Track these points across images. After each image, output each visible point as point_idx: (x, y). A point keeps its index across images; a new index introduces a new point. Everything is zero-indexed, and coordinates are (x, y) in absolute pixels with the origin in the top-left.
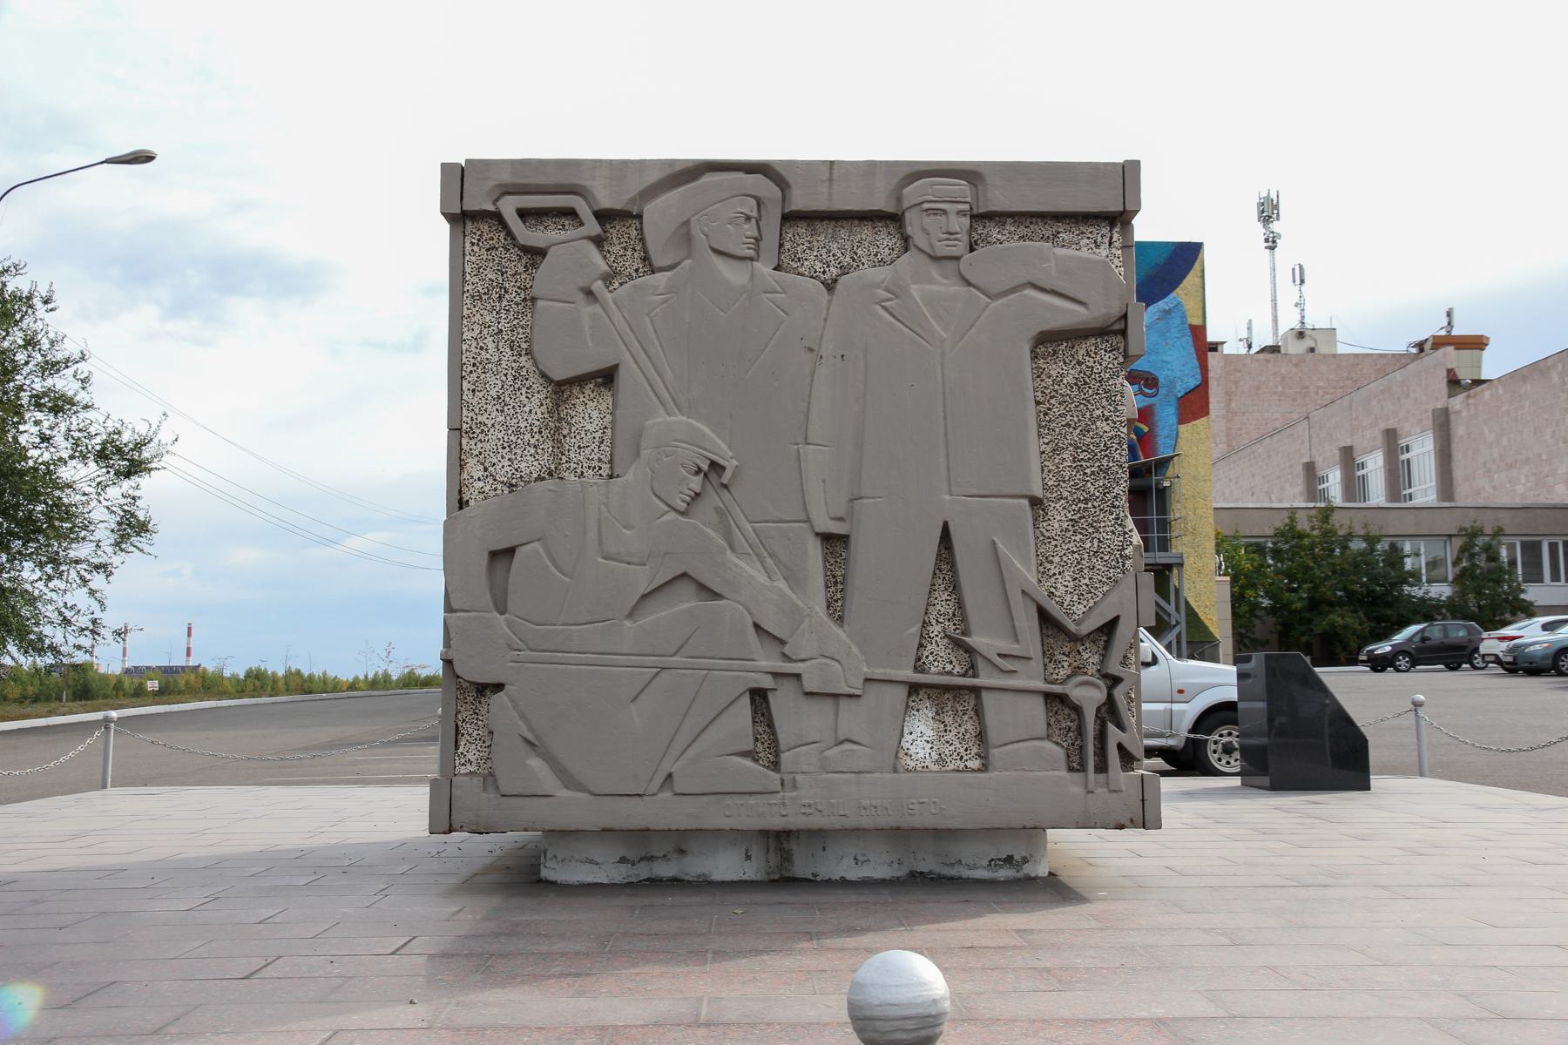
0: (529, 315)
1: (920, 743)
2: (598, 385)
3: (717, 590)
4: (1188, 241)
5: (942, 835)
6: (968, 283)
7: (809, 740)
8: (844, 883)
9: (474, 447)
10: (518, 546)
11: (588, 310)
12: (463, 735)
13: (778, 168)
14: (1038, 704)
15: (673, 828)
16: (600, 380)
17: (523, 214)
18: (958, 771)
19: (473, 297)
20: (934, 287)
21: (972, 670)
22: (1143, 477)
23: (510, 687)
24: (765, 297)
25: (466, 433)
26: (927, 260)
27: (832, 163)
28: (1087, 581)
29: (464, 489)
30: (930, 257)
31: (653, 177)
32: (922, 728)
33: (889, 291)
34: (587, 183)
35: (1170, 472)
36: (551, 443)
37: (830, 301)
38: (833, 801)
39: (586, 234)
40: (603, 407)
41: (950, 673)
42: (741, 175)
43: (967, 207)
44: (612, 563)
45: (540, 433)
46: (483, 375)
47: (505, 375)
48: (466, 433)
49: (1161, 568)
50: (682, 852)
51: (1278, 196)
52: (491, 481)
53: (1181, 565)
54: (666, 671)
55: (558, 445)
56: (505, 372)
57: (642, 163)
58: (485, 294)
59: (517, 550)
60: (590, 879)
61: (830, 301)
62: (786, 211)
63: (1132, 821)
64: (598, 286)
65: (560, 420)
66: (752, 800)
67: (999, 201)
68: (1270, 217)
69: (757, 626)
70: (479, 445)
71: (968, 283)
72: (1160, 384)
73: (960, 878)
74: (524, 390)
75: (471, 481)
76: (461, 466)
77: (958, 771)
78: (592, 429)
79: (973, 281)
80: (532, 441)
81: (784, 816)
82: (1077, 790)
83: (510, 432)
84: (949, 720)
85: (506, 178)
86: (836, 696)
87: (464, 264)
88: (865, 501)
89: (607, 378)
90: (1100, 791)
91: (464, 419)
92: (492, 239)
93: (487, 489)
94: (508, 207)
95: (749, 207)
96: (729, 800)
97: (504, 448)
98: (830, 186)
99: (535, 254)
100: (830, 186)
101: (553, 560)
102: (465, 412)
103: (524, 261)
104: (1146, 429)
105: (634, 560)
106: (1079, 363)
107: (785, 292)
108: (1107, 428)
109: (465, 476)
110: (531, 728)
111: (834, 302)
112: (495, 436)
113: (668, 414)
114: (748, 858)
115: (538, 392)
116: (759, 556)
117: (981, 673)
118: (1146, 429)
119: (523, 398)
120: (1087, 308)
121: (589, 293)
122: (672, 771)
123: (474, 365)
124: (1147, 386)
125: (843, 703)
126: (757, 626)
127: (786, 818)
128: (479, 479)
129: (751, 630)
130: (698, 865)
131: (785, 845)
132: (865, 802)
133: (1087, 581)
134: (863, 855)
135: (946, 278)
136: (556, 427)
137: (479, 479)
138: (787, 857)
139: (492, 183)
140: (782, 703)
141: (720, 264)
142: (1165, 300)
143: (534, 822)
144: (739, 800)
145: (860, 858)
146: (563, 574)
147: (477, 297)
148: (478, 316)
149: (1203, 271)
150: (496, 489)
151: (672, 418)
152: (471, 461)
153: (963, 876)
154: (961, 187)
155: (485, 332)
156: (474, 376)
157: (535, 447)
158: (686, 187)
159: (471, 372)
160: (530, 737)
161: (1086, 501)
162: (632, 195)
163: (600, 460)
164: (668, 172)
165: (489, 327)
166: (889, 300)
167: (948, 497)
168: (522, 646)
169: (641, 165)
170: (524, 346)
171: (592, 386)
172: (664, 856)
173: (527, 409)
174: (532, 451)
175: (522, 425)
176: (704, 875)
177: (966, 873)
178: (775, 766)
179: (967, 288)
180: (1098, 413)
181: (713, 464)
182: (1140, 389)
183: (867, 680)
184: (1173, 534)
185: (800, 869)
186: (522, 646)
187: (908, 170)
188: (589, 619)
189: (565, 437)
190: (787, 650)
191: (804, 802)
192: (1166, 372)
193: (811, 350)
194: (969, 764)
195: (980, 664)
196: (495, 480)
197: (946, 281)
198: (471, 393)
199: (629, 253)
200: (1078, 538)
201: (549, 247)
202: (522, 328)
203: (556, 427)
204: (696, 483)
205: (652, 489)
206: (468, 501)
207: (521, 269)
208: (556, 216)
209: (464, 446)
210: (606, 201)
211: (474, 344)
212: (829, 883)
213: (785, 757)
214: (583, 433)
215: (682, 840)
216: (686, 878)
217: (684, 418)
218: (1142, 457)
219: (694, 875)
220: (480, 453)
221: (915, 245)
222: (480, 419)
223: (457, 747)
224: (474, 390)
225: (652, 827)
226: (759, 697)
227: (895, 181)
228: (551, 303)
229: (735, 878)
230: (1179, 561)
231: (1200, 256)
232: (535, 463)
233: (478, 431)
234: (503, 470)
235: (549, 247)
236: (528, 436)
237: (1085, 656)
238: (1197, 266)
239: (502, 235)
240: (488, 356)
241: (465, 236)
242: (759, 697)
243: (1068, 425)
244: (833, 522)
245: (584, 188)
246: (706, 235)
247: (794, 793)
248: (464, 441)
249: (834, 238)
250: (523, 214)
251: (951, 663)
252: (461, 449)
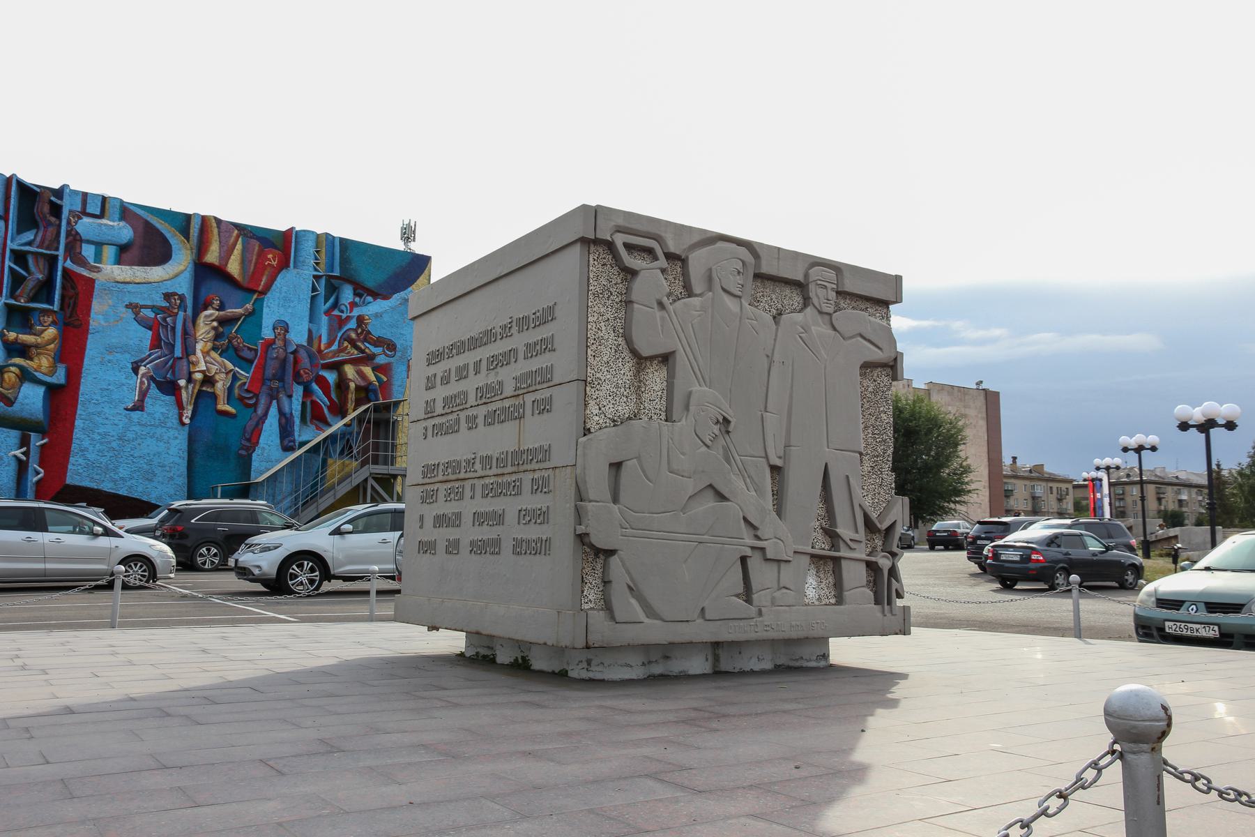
0: (624, 311)
1: (811, 589)
2: (659, 362)
3: (727, 495)
4: (421, 253)
5: (789, 642)
6: (835, 329)
7: (766, 587)
8: (752, 673)
9: (594, 394)
10: (624, 461)
11: (658, 314)
12: (586, 583)
13: (755, 246)
14: (863, 567)
15: (704, 641)
16: (660, 359)
17: (626, 246)
18: (826, 605)
19: (594, 294)
20: (819, 329)
21: (834, 547)
22: (380, 412)
23: (622, 552)
24: (747, 321)
25: (590, 383)
26: (817, 313)
27: (779, 248)
28: (877, 500)
29: (587, 420)
30: (819, 311)
31: (696, 238)
32: (811, 580)
33: (803, 328)
34: (663, 234)
35: (400, 410)
36: (635, 396)
37: (777, 329)
38: (779, 623)
39: (659, 266)
40: (662, 376)
41: (824, 549)
42: (734, 246)
43: (835, 286)
44: (675, 476)
45: (630, 388)
46: (599, 347)
47: (611, 348)
48: (590, 383)
49: (388, 476)
50: (667, 658)
51: (415, 225)
52: (603, 417)
53: (404, 476)
54: (701, 544)
55: (639, 397)
56: (610, 346)
57: (690, 228)
58: (601, 294)
59: (624, 464)
60: (627, 677)
61: (777, 329)
62: (756, 272)
63: (900, 631)
64: (665, 300)
65: (640, 381)
66: (742, 623)
67: (849, 286)
68: (409, 238)
69: (745, 519)
70: (597, 392)
71: (835, 329)
72: (397, 349)
73: (802, 667)
74: (620, 360)
75: (592, 415)
76: (585, 404)
77: (826, 605)
78: (657, 390)
79: (838, 329)
80: (625, 393)
81: (756, 632)
82: (879, 615)
83: (613, 386)
84: (822, 576)
85: (621, 222)
86: (779, 561)
87: (589, 271)
88: (792, 448)
89: (666, 359)
90: (889, 615)
91: (589, 374)
92: (604, 258)
93: (601, 421)
94: (619, 240)
95: (739, 266)
96: (731, 623)
97: (610, 396)
98: (778, 262)
99: (631, 273)
100: (778, 262)
101: (644, 471)
102: (589, 370)
103: (621, 276)
104: (385, 379)
105: (686, 474)
106: (875, 381)
107: (756, 320)
108: (885, 418)
109: (588, 412)
110: (632, 579)
111: (779, 330)
112: (605, 387)
113: (700, 385)
114: (707, 660)
115: (628, 362)
116: (743, 477)
117: (842, 550)
118: (385, 379)
119: (620, 364)
120: (882, 352)
121: (661, 305)
122: (704, 605)
123: (595, 339)
124: (388, 349)
125: (783, 565)
126: (745, 519)
127: (758, 634)
128: (596, 415)
129: (742, 521)
130: (676, 666)
131: (717, 651)
132: (794, 623)
133: (877, 500)
134: (762, 656)
135: (825, 324)
136: (638, 386)
137: (596, 415)
138: (716, 659)
139: (613, 224)
140: (755, 564)
141: (726, 298)
142: (405, 292)
143: (633, 640)
144: (736, 623)
145: (760, 657)
146: (650, 481)
147: (596, 295)
148: (597, 307)
149: (430, 276)
150: (606, 422)
151: (702, 388)
152: (592, 403)
153: (804, 666)
154: (831, 275)
155: (600, 318)
156: (595, 346)
157: (627, 397)
158: (708, 248)
159: (593, 344)
160: (632, 585)
161: (877, 456)
162: (685, 247)
163: (660, 409)
164: (704, 237)
165: (603, 316)
166: (803, 333)
167: (827, 449)
168: (628, 526)
169: (690, 229)
170: (621, 331)
171: (656, 362)
172: (656, 661)
173: (622, 372)
174: (625, 399)
175: (620, 382)
176: (684, 672)
177: (805, 664)
178: (749, 600)
179: (834, 332)
180: (882, 409)
181: (725, 419)
182: (384, 351)
183: (795, 552)
184: (399, 454)
185: (725, 666)
186: (628, 526)
187: (812, 261)
188: (663, 510)
189: (642, 392)
190: (759, 533)
191: (766, 623)
192: (401, 342)
193: (768, 356)
194: (831, 601)
195: (842, 545)
196: (605, 416)
197: (824, 326)
198: (593, 358)
199: (677, 281)
200: (874, 476)
201: (640, 270)
202: (620, 319)
203: (638, 386)
204: (716, 429)
205: (695, 431)
206: (589, 429)
207: (619, 281)
208: (639, 250)
209: (588, 392)
210: (672, 248)
211: (594, 326)
212: (742, 673)
213: (755, 597)
214: (652, 391)
215: (667, 650)
216: (670, 674)
217: (707, 389)
218: (381, 399)
219: (677, 671)
220: (597, 398)
221: (813, 304)
222: (598, 375)
223: (583, 592)
224: (594, 356)
225: (694, 641)
226: (744, 560)
227: (806, 266)
228: (641, 306)
229: (701, 673)
230: (403, 473)
231: (429, 266)
232: (627, 408)
233: (596, 383)
234: (610, 410)
235: (640, 270)
236: (623, 390)
237: (876, 541)
238: (426, 271)
239: (610, 257)
240: (602, 335)
241: (589, 253)
242: (744, 560)
243: (870, 414)
244: (777, 459)
245: (661, 237)
246: (720, 279)
247: (761, 619)
248: (588, 389)
249: (774, 291)
250: (626, 246)
251: (824, 543)
252: (586, 394)
